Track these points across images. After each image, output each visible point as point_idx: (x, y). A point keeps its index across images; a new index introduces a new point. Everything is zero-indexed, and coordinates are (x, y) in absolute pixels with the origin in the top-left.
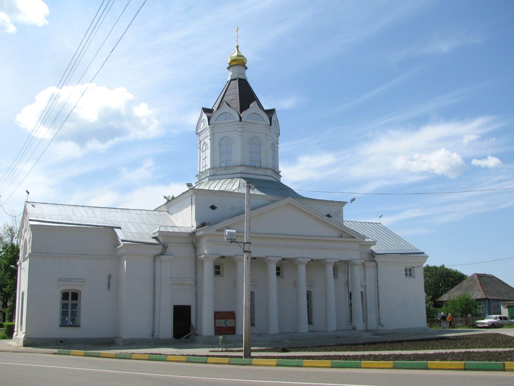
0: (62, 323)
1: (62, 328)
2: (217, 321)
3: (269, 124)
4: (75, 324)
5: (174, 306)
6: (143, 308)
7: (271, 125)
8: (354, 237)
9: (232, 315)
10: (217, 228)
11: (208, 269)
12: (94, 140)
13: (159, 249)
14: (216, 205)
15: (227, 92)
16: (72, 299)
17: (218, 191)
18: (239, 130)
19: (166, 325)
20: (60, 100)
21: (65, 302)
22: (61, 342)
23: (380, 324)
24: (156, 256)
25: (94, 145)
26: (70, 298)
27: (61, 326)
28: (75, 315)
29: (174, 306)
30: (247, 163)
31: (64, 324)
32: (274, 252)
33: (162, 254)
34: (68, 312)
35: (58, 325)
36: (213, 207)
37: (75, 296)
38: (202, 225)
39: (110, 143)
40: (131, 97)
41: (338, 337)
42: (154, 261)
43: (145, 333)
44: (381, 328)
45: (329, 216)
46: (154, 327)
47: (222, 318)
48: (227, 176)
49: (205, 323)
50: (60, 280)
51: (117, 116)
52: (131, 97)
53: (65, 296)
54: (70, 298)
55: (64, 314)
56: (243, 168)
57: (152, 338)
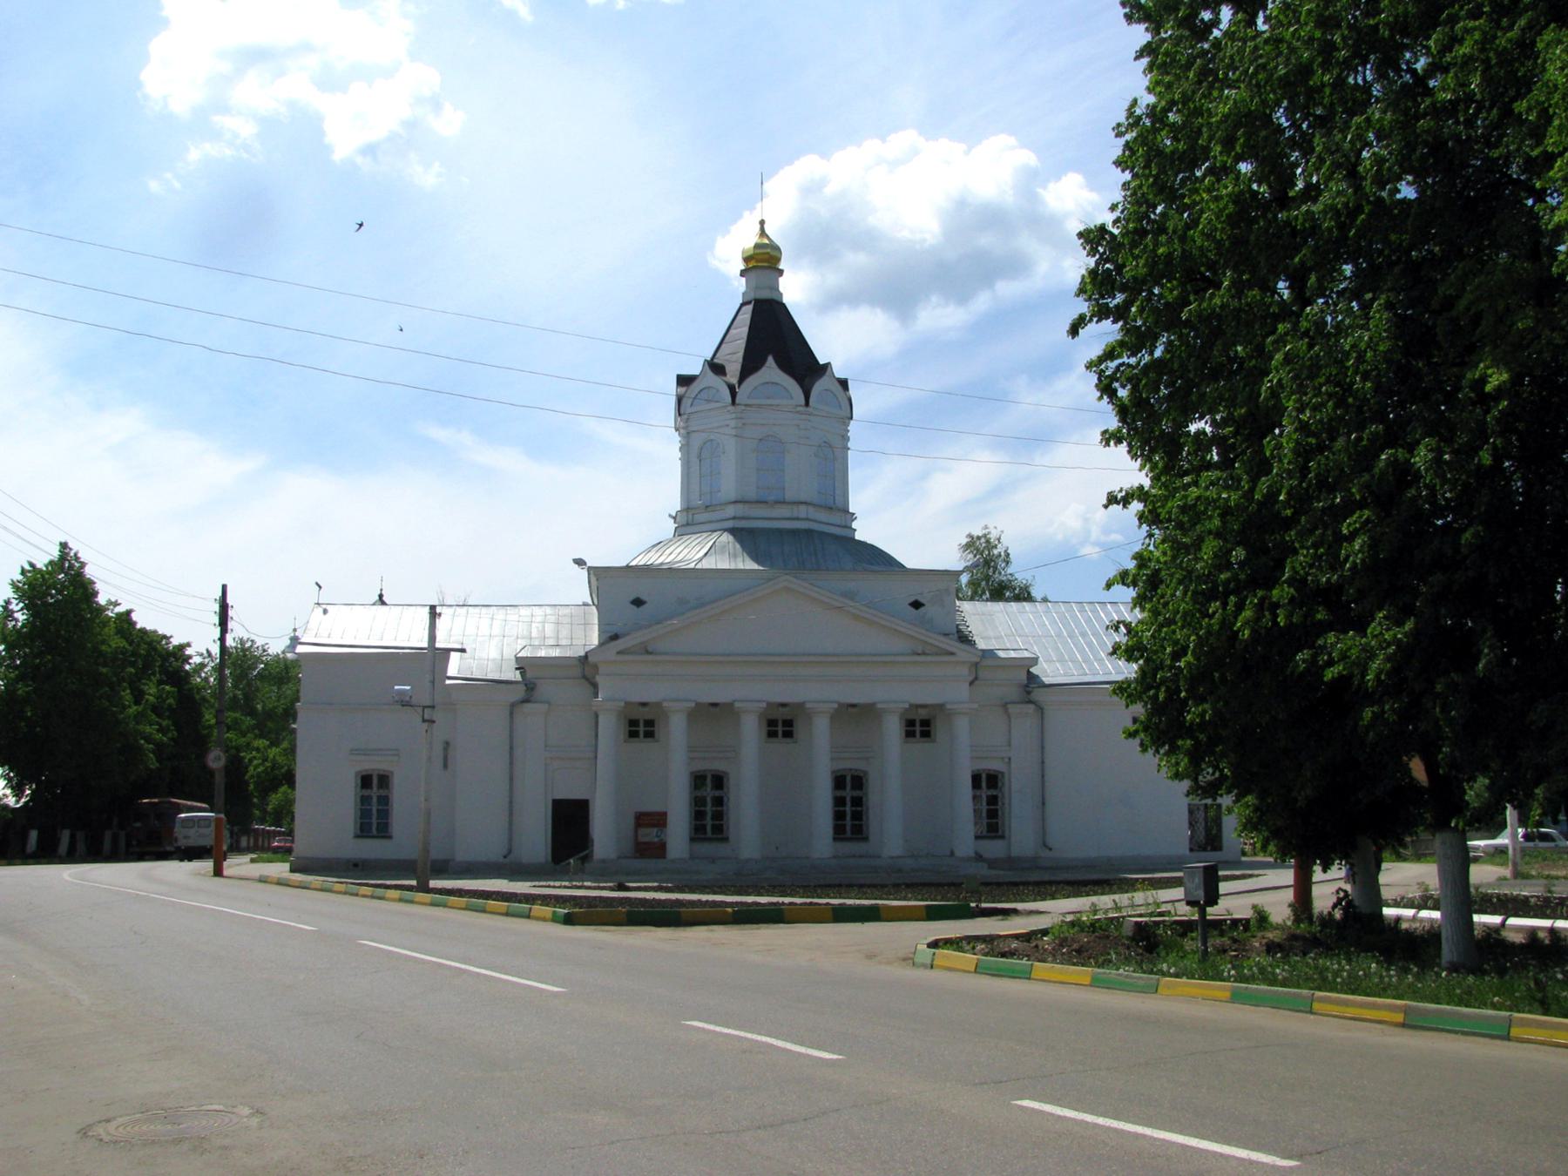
0: (362, 830)
1: (360, 841)
2: (643, 831)
3: (803, 401)
4: (384, 831)
5: (557, 804)
6: (492, 801)
7: (807, 404)
8: (952, 654)
9: (658, 820)
10: (621, 647)
11: (610, 727)
12: (934, 299)
13: (520, 693)
14: (644, 598)
15: (732, 331)
16: (853, 788)
17: (628, 567)
18: (733, 424)
19: (536, 838)
20: (828, 191)
21: (840, 793)
22: (356, 865)
23: (1045, 845)
24: (513, 705)
25: (939, 317)
26: (984, 784)
27: (357, 836)
28: (385, 814)
29: (557, 804)
30: (752, 494)
31: (364, 831)
32: (755, 692)
33: (526, 701)
34: (713, 819)
35: (352, 834)
36: (638, 602)
37: (384, 780)
38: (610, 637)
39: (982, 302)
40: (1028, 158)
41: (900, 871)
42: (511, 714)
43: (492, 850)
44: (1045, 853)
45: (917, 605)
46: (510, 840)
47: (653, 826)
48: (714, 526)
49: (606, 832)
50: (354, 751)
51: (992, 218)
52: (1028, 158)
53: (365, 781)
54: (984, 784)
55: (364, 814)
56: (740, 506)
57: (501, 860)
